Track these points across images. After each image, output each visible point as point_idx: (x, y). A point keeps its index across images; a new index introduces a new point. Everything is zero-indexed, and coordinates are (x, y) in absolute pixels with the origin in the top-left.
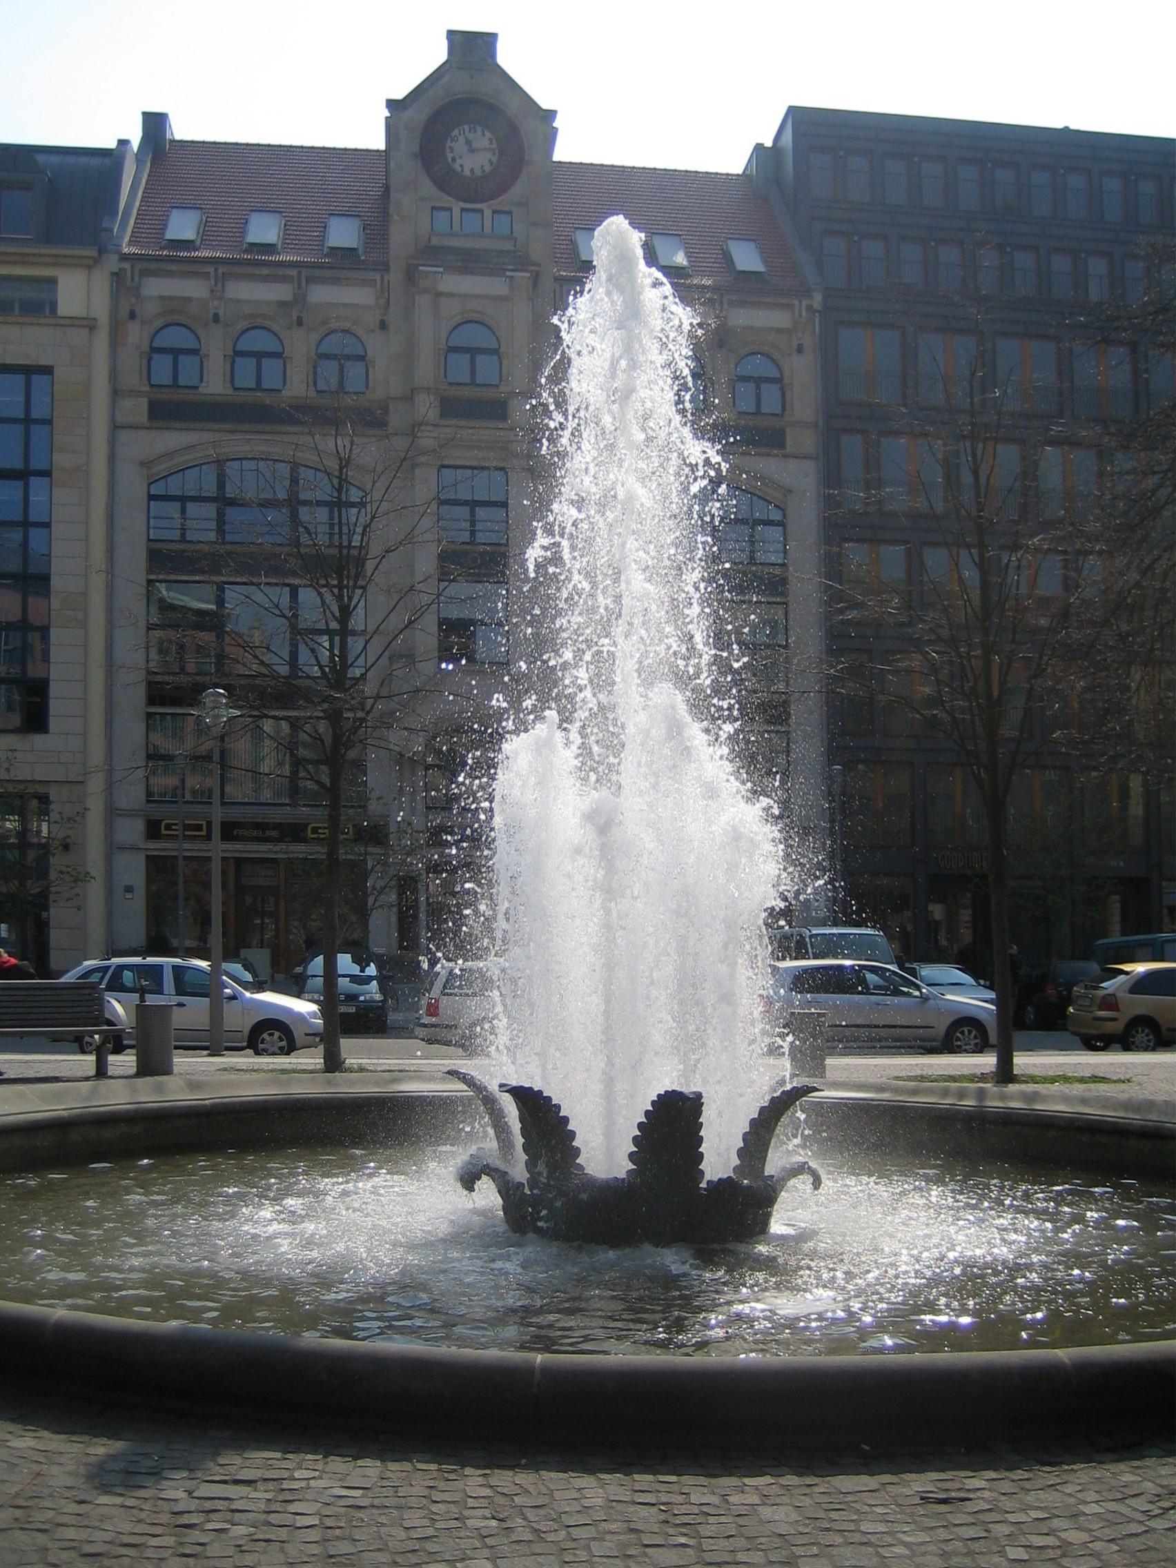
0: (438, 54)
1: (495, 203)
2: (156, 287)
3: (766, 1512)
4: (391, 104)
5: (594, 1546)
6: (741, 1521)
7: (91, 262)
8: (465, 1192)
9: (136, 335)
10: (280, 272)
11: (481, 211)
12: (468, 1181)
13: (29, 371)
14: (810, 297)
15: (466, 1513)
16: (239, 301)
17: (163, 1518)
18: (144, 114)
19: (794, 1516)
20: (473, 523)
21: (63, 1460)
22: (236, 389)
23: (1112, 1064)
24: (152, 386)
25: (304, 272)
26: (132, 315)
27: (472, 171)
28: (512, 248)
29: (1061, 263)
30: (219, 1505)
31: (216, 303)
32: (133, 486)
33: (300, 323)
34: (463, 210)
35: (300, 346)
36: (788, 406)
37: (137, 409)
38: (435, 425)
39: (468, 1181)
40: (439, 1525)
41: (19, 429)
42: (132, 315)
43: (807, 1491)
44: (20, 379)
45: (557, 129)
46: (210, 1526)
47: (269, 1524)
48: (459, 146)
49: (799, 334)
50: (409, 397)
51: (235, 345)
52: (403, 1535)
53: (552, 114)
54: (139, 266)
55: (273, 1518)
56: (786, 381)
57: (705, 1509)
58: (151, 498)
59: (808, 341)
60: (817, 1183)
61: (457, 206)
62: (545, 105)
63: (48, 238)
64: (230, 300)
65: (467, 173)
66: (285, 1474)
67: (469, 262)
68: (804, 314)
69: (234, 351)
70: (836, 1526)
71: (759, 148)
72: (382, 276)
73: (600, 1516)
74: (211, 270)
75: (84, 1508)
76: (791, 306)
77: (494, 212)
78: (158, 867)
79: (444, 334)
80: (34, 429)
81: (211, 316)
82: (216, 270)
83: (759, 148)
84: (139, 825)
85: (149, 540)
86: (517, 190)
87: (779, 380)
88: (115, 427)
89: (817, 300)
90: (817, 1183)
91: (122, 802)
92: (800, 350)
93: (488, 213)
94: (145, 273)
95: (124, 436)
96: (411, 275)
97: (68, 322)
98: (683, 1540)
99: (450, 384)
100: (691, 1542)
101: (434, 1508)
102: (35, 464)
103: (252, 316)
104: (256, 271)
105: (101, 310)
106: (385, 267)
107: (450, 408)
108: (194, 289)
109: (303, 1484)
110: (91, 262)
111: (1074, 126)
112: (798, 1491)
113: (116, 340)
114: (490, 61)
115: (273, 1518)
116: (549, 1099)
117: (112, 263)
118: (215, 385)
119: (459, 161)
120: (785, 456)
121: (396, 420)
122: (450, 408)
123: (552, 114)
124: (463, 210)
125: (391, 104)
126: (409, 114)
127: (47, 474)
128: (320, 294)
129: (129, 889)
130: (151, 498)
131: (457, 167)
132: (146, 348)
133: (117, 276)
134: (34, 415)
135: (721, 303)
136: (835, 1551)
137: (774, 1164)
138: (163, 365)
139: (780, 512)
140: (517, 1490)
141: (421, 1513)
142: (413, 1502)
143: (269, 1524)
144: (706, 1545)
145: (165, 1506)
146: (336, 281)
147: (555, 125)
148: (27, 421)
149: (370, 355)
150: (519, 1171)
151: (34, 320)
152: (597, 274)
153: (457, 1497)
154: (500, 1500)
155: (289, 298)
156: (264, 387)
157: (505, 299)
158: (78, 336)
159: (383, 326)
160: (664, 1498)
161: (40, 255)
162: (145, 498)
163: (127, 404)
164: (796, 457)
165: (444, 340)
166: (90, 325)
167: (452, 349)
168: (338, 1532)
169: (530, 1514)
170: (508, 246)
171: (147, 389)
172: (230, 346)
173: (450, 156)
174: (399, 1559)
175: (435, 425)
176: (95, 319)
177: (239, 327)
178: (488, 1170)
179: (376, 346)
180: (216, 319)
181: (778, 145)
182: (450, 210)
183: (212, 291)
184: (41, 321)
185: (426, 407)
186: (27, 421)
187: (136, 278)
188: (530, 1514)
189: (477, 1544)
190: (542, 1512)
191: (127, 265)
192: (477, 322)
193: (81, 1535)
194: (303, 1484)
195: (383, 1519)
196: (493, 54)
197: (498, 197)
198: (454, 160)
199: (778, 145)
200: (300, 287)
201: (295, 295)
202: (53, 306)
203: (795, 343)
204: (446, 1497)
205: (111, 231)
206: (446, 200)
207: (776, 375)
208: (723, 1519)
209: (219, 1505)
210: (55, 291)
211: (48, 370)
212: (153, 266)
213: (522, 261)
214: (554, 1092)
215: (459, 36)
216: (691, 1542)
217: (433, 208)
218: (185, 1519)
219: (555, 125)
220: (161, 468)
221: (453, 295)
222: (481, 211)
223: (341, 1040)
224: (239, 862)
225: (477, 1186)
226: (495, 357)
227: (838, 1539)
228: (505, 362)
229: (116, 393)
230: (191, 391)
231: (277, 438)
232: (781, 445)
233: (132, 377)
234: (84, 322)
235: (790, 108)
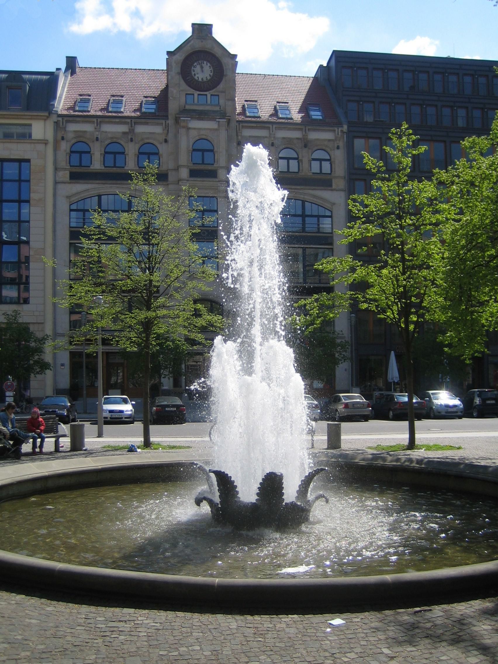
0: (189, 32)
1: (212, 92)
2: (72, 127)
3: (287, 630)
4: (169, 53)
6: (279, 633)
7: (45, 118)
8: (196, 506)
9: (64, 146)
10: (123, 120)
11: (206, 95)
12: (198, 502)
13: (20, 161)
14: (342, 127)
15: (192, 631)
16: (106, 132)
17: (98, 634)
18: (67, 57)
19: (296, 631)
20: (84, 219)
21: (64, 614)
22: (105, 167)
24: (71, 166)
25: (133, 120)
26: (63, 138)
27: (202, 79)
28: (219, 110)
29: (447, 111)
30: (115, 629)
31: (97, 133)
32: (64, 206)
33: (132, 140)
34: (199, 95)
36: (333, 170)
37: (65, 175)
38: (188, 180)
39: (198, 502)
40: (184, 635)
41: (17, 184)
42: (63, 138)
43: (302, 623)
44: (17, 164)
45: (237, 62)
46: (112, 636)
47: (130, 635)
48: (198, 69)
49: (338, 142)
50: (177, 169)
51: (105, 149)
52: (172, 638)
53: (235, 56)
54: (65, 119)
55: (132, 633)
56: (332, 160)
57: (268, 629)
58: (71, 210)
59: (341, 144)
60: (327, 501)
61: (196, 93)
62: (232, 52)
63: (28, 108)
64: (103, 132)
65: (200, 80)
66: (135, 619)
67: (201, 115)
68: (340, 134)
69: (105, 152)
70: (308, 634)
71: (321, 67)
72: (165, 122)
73: (235, 631)
74: (95, 120)
75: (73, 631)
76: (334, 131)
77: (211, 95)
78: (73, 354)
79: (191, 144)
80: (23, 184)
81: (95, 138)
82: (97, 120)
83: (321, 67)
84: (66, 339)
85: (70, 227)
86: (221, 86)
87: (329, 160)
88: (56, 183)
89: (345, 128)
90: (327, 501)
91: (60, 330)
92: (338, 148)
93: (209, 96)
94: (68, 121)
95: (59, 186)
96: (177, 120)
97: (36, 142)
98: (260, 639)
99: (194, 164)
100: (262, 640)
101: (183, 629)
102: (23, 198)
103: (112, 138)
104: (114, 120)
105: (50, 136)
106: (166, 117)
107: (194, 173)
108: (88, 128)
109: (141, 622)
110: (45, 118)
111: (452, 56)
113: (56, 148)
114: (209, 35)
115: (132, 633)
116: (227, 475)
117: (54, 118)
118: (97, 165)
119: (197, 76)
120: (332, 190)
121: (171, 178)
122: (194, 173)
123: (235, 56)
124: (199, 95)
125: (169, 53)
126: (175, 57)
127: (28, 201)
128: (140, 129)
129: (63, 365)
130: (71, 210)
131: (196, 78)
132: (68, 151)
133: (56, 123)
134: (22, 178)
135: (305, 130)
136: (307, 642)
137: (310, 496)
138: (76, 157)
139: (330, 212)
140: (209, 623)
141: (178, 631)
142: (176, 628)
143: (130, 635)
145: (98, 630)
146: (146, 124)
147: (236, 60)
148: (20, 181)
149: (161, 152)
150: (217, 499)
151: (22, 141)
152: (216, 350)
153: (190, 625)
154: (203, 626)
155: (127, 130)
156: (117, 165)
157: (216, 130)
158: (41, 147)
159: (166, 141)
161: (24, 115)
162: (69, 210)
163: (61, 174)
164: (337, 190)
165: (191, 147)
166: (45, 142)
167: (194, 150)
168: (152, 638)
169: (213, 631)
170: (217, 109)
171: (69, 167)
172: (103, 150)
173: (193, 73)
175: (188, 180)
176: (48, 140)
177: (107, 142)
178: (205, 499)
179: (163, 149)
180: (97, 139)
181: (329, 65)
182: (193, 94)
183: (95, 128)
184: (25, 141)
185: (184, 173)
186: (20, 181)
187: (64, 123)
188: (213, 631)
189: (196, 641)
190: (217, 630)
191: (60, 119)
192: (204, 139)
194: (141, 622)
195: (167, 633)
196: (211, 33)
197: (213, 89)
198: (195, 75)
199: (329, 65)
200: (131, 126)
201: (129, 129)
202: (30, 136)
203: (336, 146)
205: (54, 105)
206: (191, 91)
207: (329, 158)
208: (273, 632)
209: (115, 629)
210: (31, 129)
211: (28, 161)
212: (71, 119)
213: (223, 114)
214: (230, 472)
215: (196, 26)
216: (262, 640)
217: (186, 94)
218: (105, 634)
219: (236, 60)
220: (74, 199)
221: (195, 129)
222: (206, 95)
223: (150, 426)
224: (107, 353)
225: (201, 504)
226: (212, 153)
227: (308, 639)
228: (216, 155)
229: (56, 169)
230: (87, 168)
231: (123, 186)
232: (331, 186)
233: (63, 162)
234: (43, 142)
235: (334, 52)
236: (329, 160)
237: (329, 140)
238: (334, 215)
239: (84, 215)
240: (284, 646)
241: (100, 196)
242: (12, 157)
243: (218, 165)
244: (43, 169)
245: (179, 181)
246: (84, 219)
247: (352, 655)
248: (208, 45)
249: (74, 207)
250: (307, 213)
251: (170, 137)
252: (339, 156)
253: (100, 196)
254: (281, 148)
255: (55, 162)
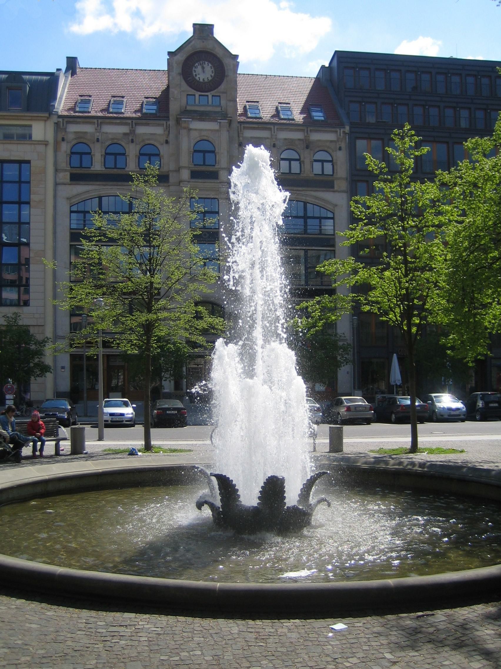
0: (190, 32)
1: (213, 93)
2: (73, 128)
3: (289, 635)
4: (170, 53)
5: (234, 646)
6: (281, 638)
7: (46, 119)
8: (197, 510)
9: (65, 147)
10: (124, 121)
11: (207, 96)
12: (199, 506)
13: (20, 162)
14: (344, 128)
15: (194, 635)
16: (107, 133)
17: (99, 638)
18: (67, 58)
20: (85, 221)
21: (64, 619)
22: (106, 168)
23: (461, 441)
24: (71, 167)
25: (134, 121)
26: (63, 139)
27: (203, 79)
28: (220, 110)
29: (449, 112)
30: (116, 634)
31: (98, 134)
32: (64, 207)
33: (132, 141)
34: (200, 95)
35: (132, 151)
36: (335, 171)
37: (65, 176)
38: (189, 182)
39: (199, 506)
40: (185, 640)
41: (17, 185)
42: (63, 139)
43: (304, 627)
44: (17, 166)
45: (239, 62)
46: (113, 641)
48: (199, 69)
49: (340, 143)
50: (178, 170)
51: (106, 151)
52: (173, 643)
53: (236, 57)
54: (66, 120)
55: (133, 638)
56: (334, 161)
57: (269, 634)
58: (72, 212)
59: (343, 145)
60: (329, 505)
61: (197, 94)
62: (234, 52)
63: (28, 108)
64: (103, 133)
65: (201, 80)
66: (136, 623)
67: (203, 116)
68: (342, 135)
69: (105, 153)
70: (310, 639)
71: (323, 67)
72: (166, 123)
73: (236, 636)
74: (96, 121)
75: (73, 635)
76: (336, 132)
77: (213, 96)
78: (73, 357)
79: (192, 145)
80: (23, 185)
81: (96, 139)
82: (98, 121)
83: (323, 67)
84: (66, 342)
85: (71, 229)
86: (222, 87)
87: (331, 161)
88: (56, 184)
89: (347, 129)
90: (329, 505)
91: (60, 333)
92: (340, 149)
93: (210, 97)
94: (68, 122)
95: (60, 188)
96: (178, 121)
97: (37, 143)
98: (261, 644)
100: (264, 645)
102: (23, 199)
103: (112, 139)
104: (115, 121)
105: (50, 137)
106: (167, 118)
107: (195, 175)
108: (89, 129)
109: (142, 627)
110: (46, 119)
111: (455, 57)
112: (300, 628)
113: (56, 149)
114: (211, 36)
115: (133, 638)
116: (229, 478)
117: (55, 119)
118: (98, 166)
119: (198, 76)
120: (334, 192)
121: (172, 180)
123: (236, 57)
124: (200, 95)
125: (170, 53)
126: (176, 58)
127: (28, 203)
128: (141, 130)
129: (63, 368)
130: (72, 212)
131: (197, 78)
132: (69, 152)
133: (57, 124)
134: (23, 180)
135: (307, 131)
136: (309, 647)
137: (312, 500)
138: (76, 158)
139: (332, 214)
140: (210, 628)
141: (179, 636)
143: (131, 640)
144: (268, 645)
145: (99, 635)
146: (147, 125)
147: (238, 61)
148: (20, 182)
149: (162, 153)
150: (218, 503)
151: (22, 142)
152: (217, 353)
153: (192, 630)
154: (205, 631)
155: (128, 131)
156: (118, 167)
157: (217, 131)
158: (41, 148)
159: (167, 142)
160: (257, 630)
161: (24, 116)
162: (69, 212)
163: (61, 175)
164: (339, 192)
165: (192, 148)
166: (46, 143)
167: (195, 151)
168: (153, 642)
169: (214, 636)
170: (219, 109)
171: (69, 169)
172: (104, 151)
173: (194, 74)
174: (172, 651)
175: (189, 182)
176: (48, 141)
177: (108, 143)
178: (206, 502)
179: (164, 150)
180: (98, 140)
181: (331, 66)
182: (195, 95)
183: (96, 129)
184: (25, 142)
185: (185, 174)
186: (20, 182)
187: (65, 124)
188: (214, 636)
189: (197, 646)
190: (218, 635)
191: (61, 120)
192: (205, 140)
193: (74, 644)
194: (142, 627)
195: (168, 638)
196: (212, 33)
197: (214, 90)
198: (196, 75)
199: (331, 66)
200: (132, 127)
201: (130, 130)
202: (30, 137)
203: (338, 147)
204: (188, 630)
205: (54, 106)
206: (193, 92)
207: (331, 159)
208: (275, 637)
209: (116, 634)
210: (31, 130)
211: (28, 162)
212: (71, 120)
213: (224, 115)
214: (231, 476)
215: (198, 26)
216: (264, 645)
217: (187, 95)
218: (105, 639)
219: (238, 61)
220: (75, 200)
221: (196, 130)
223: (151, 429)
224: (108, 356)
225: (203, 508)
226: (214, 154)
227: (310, 644)
228: (217, 156)
229: (57, 170)
230: (87, 169)
231: (124, 187)
232: (333, 187)
233: (63, 164)
234: (43, 143)
235: (336, 52)
236: (331, 161)
237: (331, 141)
238: (336, 217)
239: (85, 217)
240: (285, 651)
241: (100, 198)
242: (12, 158)
243: (219, 167)
244: (44, 171)
245: (180, 182)
246: (85, 221)
247: (354, 660)
248: (209, 46)
249: (74, 208)
250: (309, 214)
251: (171, 138)
252: (341, 157)
253: (100, 198)
254: (283, 149)
255: (55, 163)
